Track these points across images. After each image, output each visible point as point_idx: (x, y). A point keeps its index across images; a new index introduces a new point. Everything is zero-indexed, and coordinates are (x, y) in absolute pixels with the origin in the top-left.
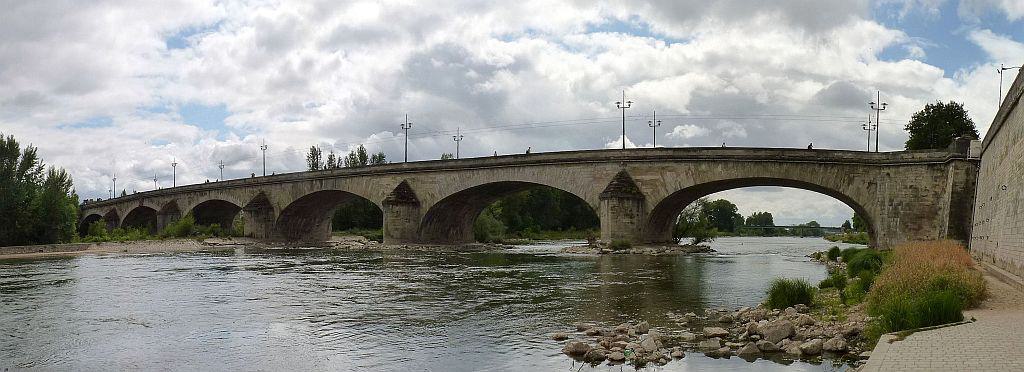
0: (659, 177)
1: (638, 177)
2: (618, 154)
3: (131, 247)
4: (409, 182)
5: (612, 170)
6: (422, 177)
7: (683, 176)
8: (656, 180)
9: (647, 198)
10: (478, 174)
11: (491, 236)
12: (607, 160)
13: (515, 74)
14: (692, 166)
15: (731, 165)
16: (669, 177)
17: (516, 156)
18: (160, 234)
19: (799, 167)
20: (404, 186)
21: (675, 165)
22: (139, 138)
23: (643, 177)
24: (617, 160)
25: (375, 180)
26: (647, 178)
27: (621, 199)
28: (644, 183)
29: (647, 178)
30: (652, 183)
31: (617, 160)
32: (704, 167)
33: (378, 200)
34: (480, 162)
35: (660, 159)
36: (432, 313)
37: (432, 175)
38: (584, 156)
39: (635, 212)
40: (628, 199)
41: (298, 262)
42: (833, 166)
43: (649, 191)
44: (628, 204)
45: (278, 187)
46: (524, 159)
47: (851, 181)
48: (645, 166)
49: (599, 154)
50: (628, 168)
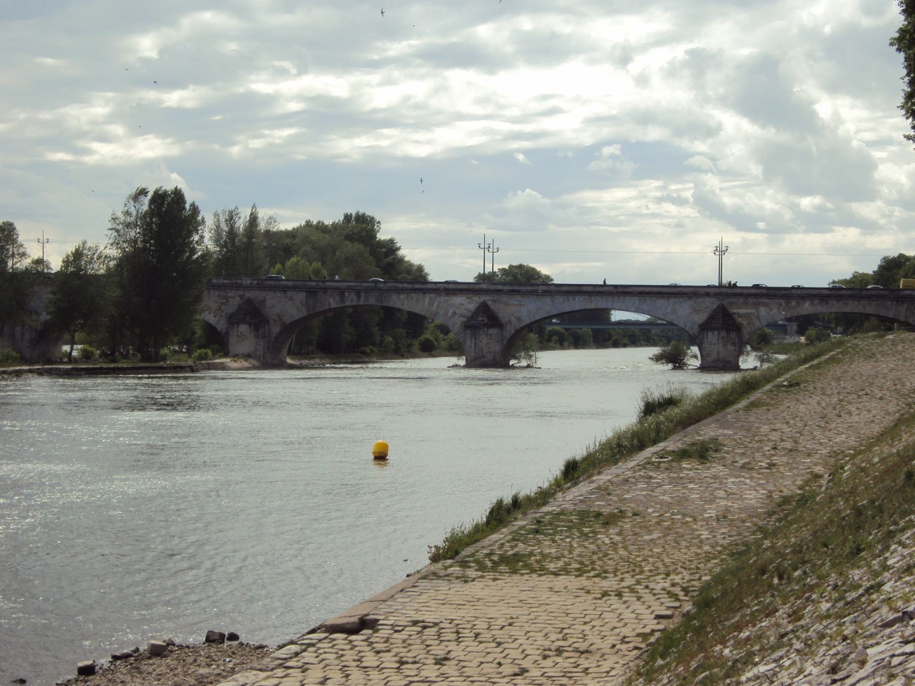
1: (735, 311)
2: (717, 291)
4: (489, 303)
5: (710, 304)
6: (505, 298)
10: (574, 299)
11: (731, 398)
13: (422, 267)
15: (816, 302)
16: (763, 311)
21: (767, 301)
22: (582, 589)
23: (740, 311)
25: (442, 298)
28: (740, 315)
30: (747, 316)
31: (716, 295)
36: (246, 364)
37: (518, 298)
40: (733, 330)
41: (160, 547)
43: (745, 323)
45: (279, 294)
46: (601, 289)
48: (742, 300)
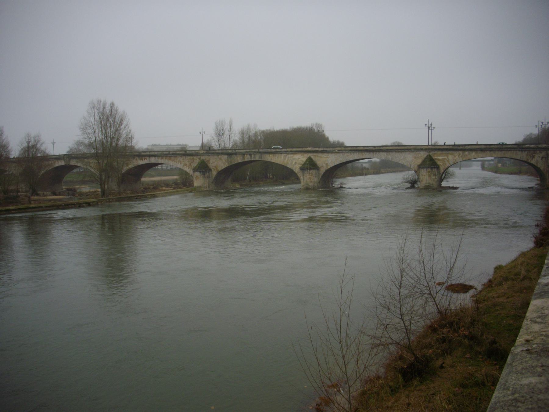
0: (446, 157)
1: (436, 158)
3: (172, 149)
4: (312, 157)
6: (320, 155)
7: (457, 157)
8: (445, 159)
9: (440, 167)
12: (422, 150)
14: (461, 153)
17: (374, 147)
18: (524, 328)
19: (510, 152)
20: (310, 159)
23: (439, 157)
24: (426, 150)
25: (290, 156)
26: (440, 158)
27: (432, 168)
28: (439, 160)
29: (440, 158)
30: (443, 160)
31: (426, 150)
32: (467, 153)
33: (296, 169)
34: (355, 148)
35: (447, 150)
38: (409, 148)
39: (437, 174)
40: (434, 168)
42: (525, 151)
43: (441, 164)
44: (435, 170)
47: (533, 157)
49: (417, 147)
50: (431, 153)
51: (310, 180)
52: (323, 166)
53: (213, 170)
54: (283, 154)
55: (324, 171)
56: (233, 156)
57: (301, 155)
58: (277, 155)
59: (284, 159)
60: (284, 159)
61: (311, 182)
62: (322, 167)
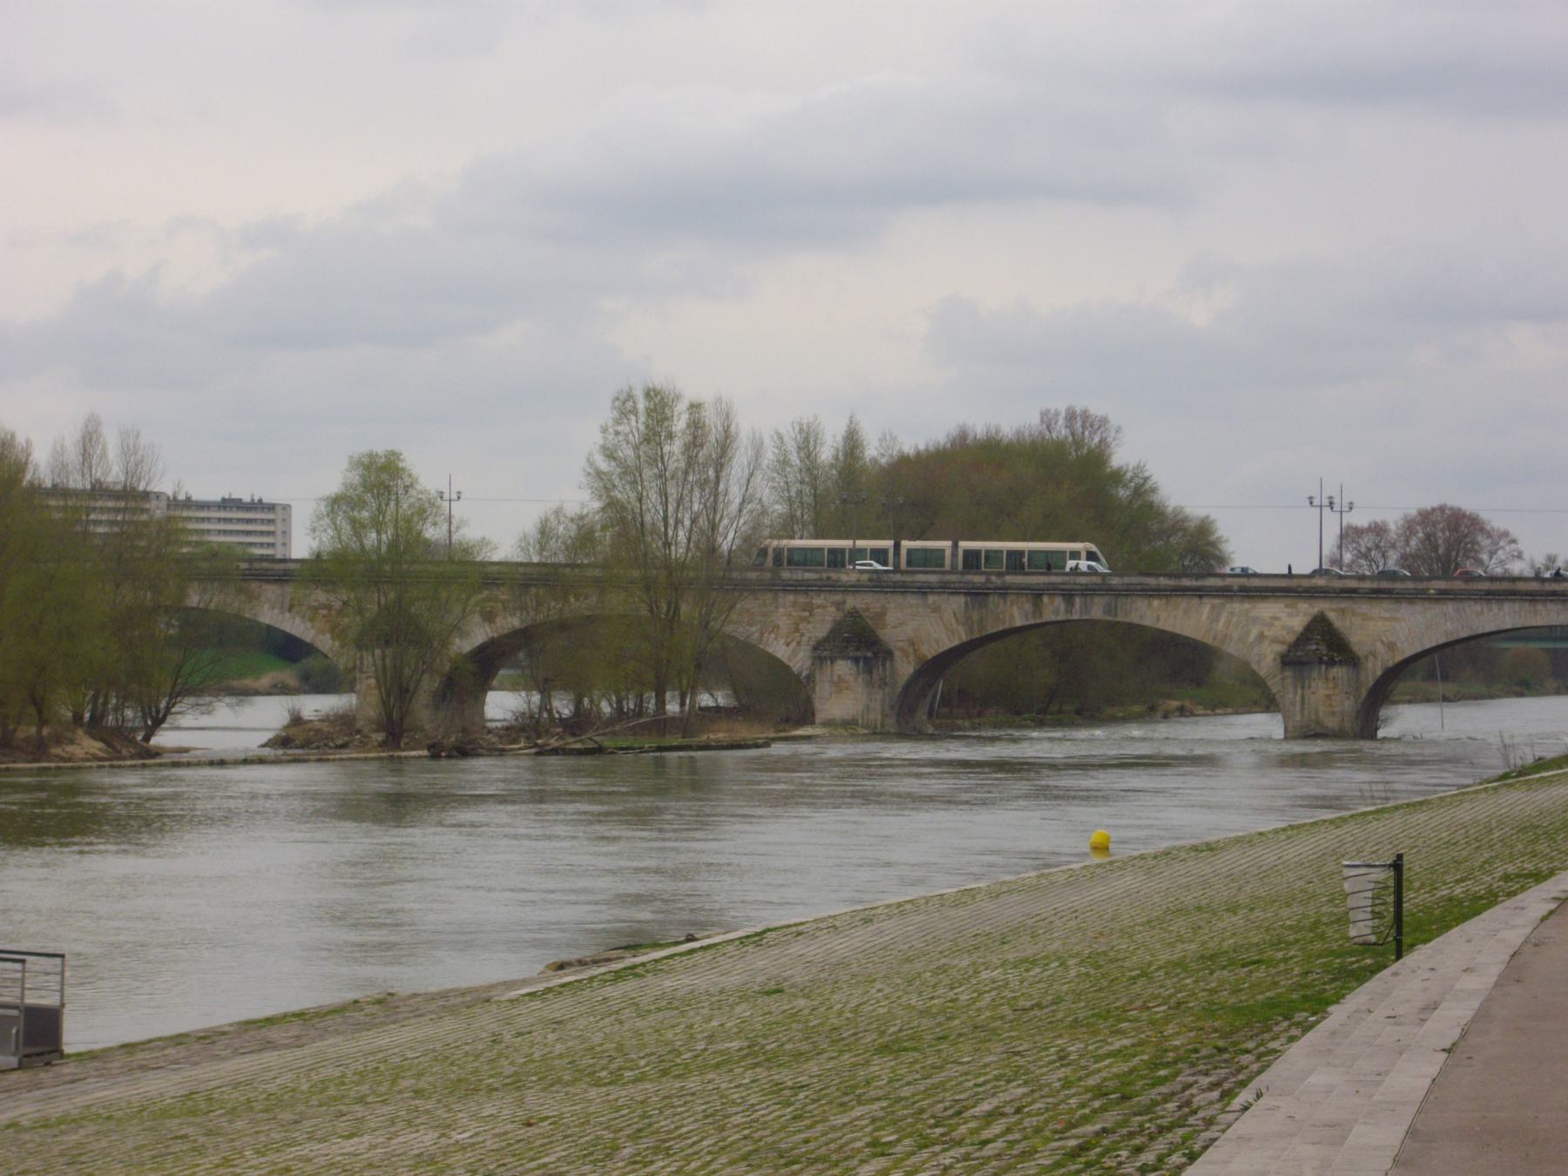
4: (1332, 616)
51: (1330, 705)
52: (1373, 654)
53: (897, 654)
54: (1205, 600)
55: (1379, 673)
56: (993, 600)
57: (1286, 606)
58: (1183, 603)
59: (1214, 619)
60: (1214, 619)
61: (1333, 713)
62: (1371, 658)
